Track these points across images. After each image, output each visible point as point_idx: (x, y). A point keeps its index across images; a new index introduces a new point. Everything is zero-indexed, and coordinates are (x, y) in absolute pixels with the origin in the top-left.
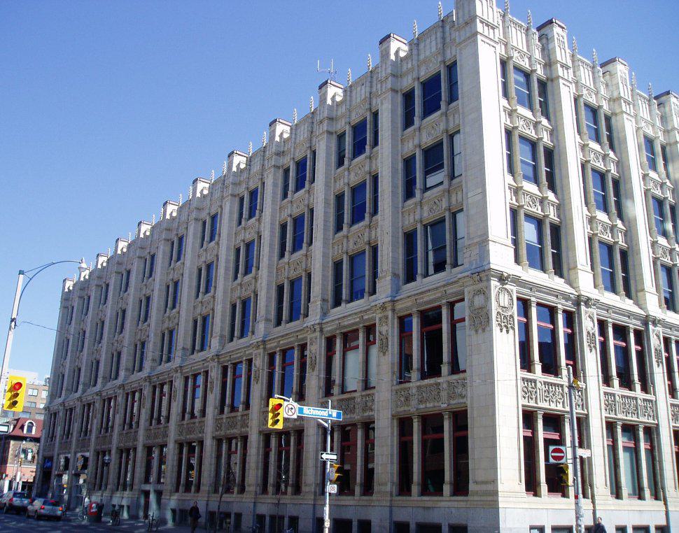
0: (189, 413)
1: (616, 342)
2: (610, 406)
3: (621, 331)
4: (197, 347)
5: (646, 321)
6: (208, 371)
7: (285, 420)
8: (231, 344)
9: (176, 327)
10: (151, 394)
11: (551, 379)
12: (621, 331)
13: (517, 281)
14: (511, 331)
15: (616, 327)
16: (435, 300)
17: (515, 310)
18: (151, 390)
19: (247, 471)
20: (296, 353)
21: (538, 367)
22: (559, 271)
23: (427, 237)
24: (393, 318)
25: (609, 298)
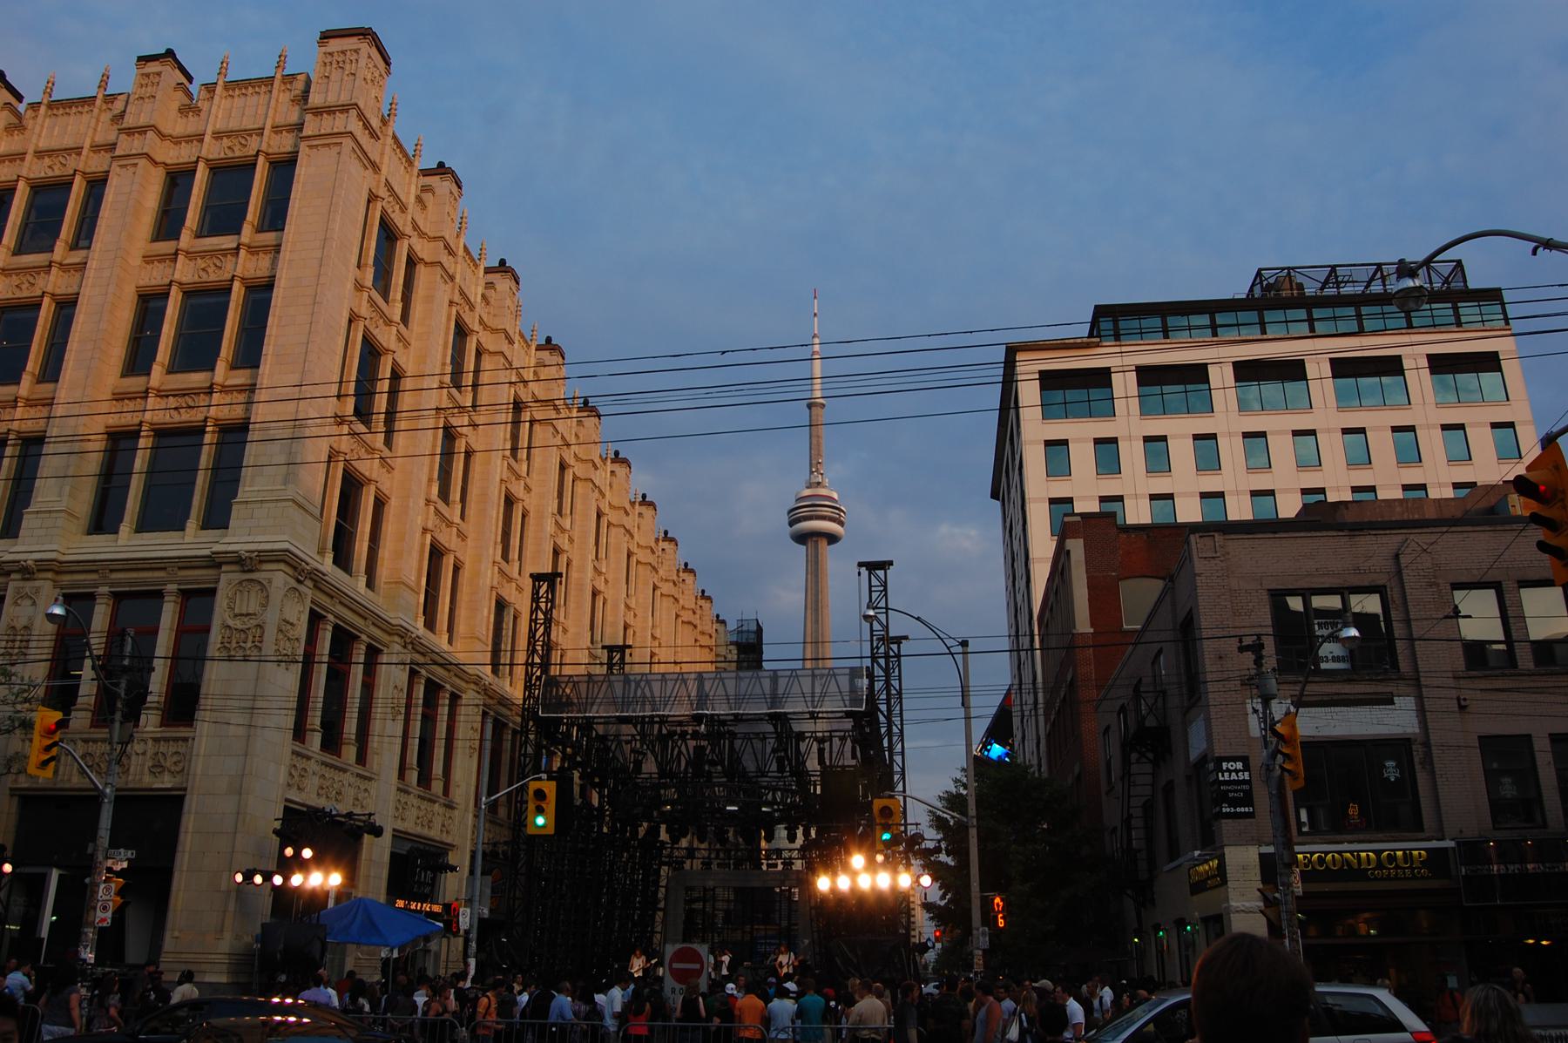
2: (296, 778)
11: (329, 758)
12: (343, 639)
20: (169, 615)
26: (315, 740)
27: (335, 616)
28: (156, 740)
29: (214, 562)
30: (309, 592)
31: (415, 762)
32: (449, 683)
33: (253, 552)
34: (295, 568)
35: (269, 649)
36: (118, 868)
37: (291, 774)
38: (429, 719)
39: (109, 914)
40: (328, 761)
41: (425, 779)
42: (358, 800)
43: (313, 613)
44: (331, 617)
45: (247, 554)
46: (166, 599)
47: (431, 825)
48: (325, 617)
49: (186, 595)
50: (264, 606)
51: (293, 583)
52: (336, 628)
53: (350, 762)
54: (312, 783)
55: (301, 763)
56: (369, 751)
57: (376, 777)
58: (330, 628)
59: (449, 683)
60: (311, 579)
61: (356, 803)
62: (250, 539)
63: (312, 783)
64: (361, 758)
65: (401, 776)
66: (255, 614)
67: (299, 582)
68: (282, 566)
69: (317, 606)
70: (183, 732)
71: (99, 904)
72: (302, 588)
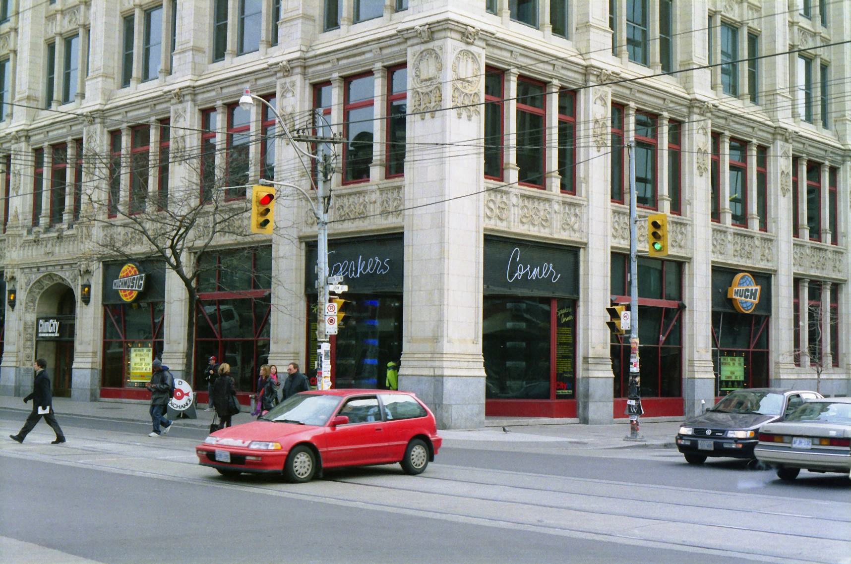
0: (125, 204)
1: (810, 183)
2: (798, 262)
3: (740, 145)
4: (58, 94)
5: (693, 104)
6: (81, 139)
7: (206, 389)
8: (218, 65)
9: (12, 56)
10: (30, 171)
11: (493, 183)
12: (740, 145)
13: (489, 39)
14: (704, 174)
15: (810, 162)
16: (62, 137)
17: (480, 85)
18: (31, 158)
19: (336, 232)
21: (513, 175)
22: (559, 27)
23: (497, 61)
24: (303, 88)
25: (632, 70)
26: (806, 233)
27: (560, 80)
28: (382, 191)
29: (404, 36)
30: (480, 50)
31: (827, 227)
32: (633, 100)
33: (425, 25)
34: (463, 34)
35: (448, 103)
36: (339, 291)
37: (614, 228)
38: (814, 192)
39: (335, 325)
40: (527, 193)
41: (741, 219)
42: (764, 256)
43: (615, 104)
44: (515, 70)
45: (421, 29)
46: (376, 75)
47: (824, 267)
48: (823, 163)
49: (347, 80)
50: (440, 69)
51: (464, 46)
52: (521, 77)
53: (755, 231)
54: (515, 213)
55: (720, 236)
56: (577, 182)
57: (585, 203)
58: (827, 169)
59: (556, 78)
60: (480, 38)
61: (763, 258)
62: (421, 15)
63: (730, 248)
64: (764, 227)
65: (796, 234)
66: (435, 78)
67: (468, 43)
68: (449, 34)
69: (492, 60)
70: (396, 182)
71: (327, 318)
72: (472, 49)
